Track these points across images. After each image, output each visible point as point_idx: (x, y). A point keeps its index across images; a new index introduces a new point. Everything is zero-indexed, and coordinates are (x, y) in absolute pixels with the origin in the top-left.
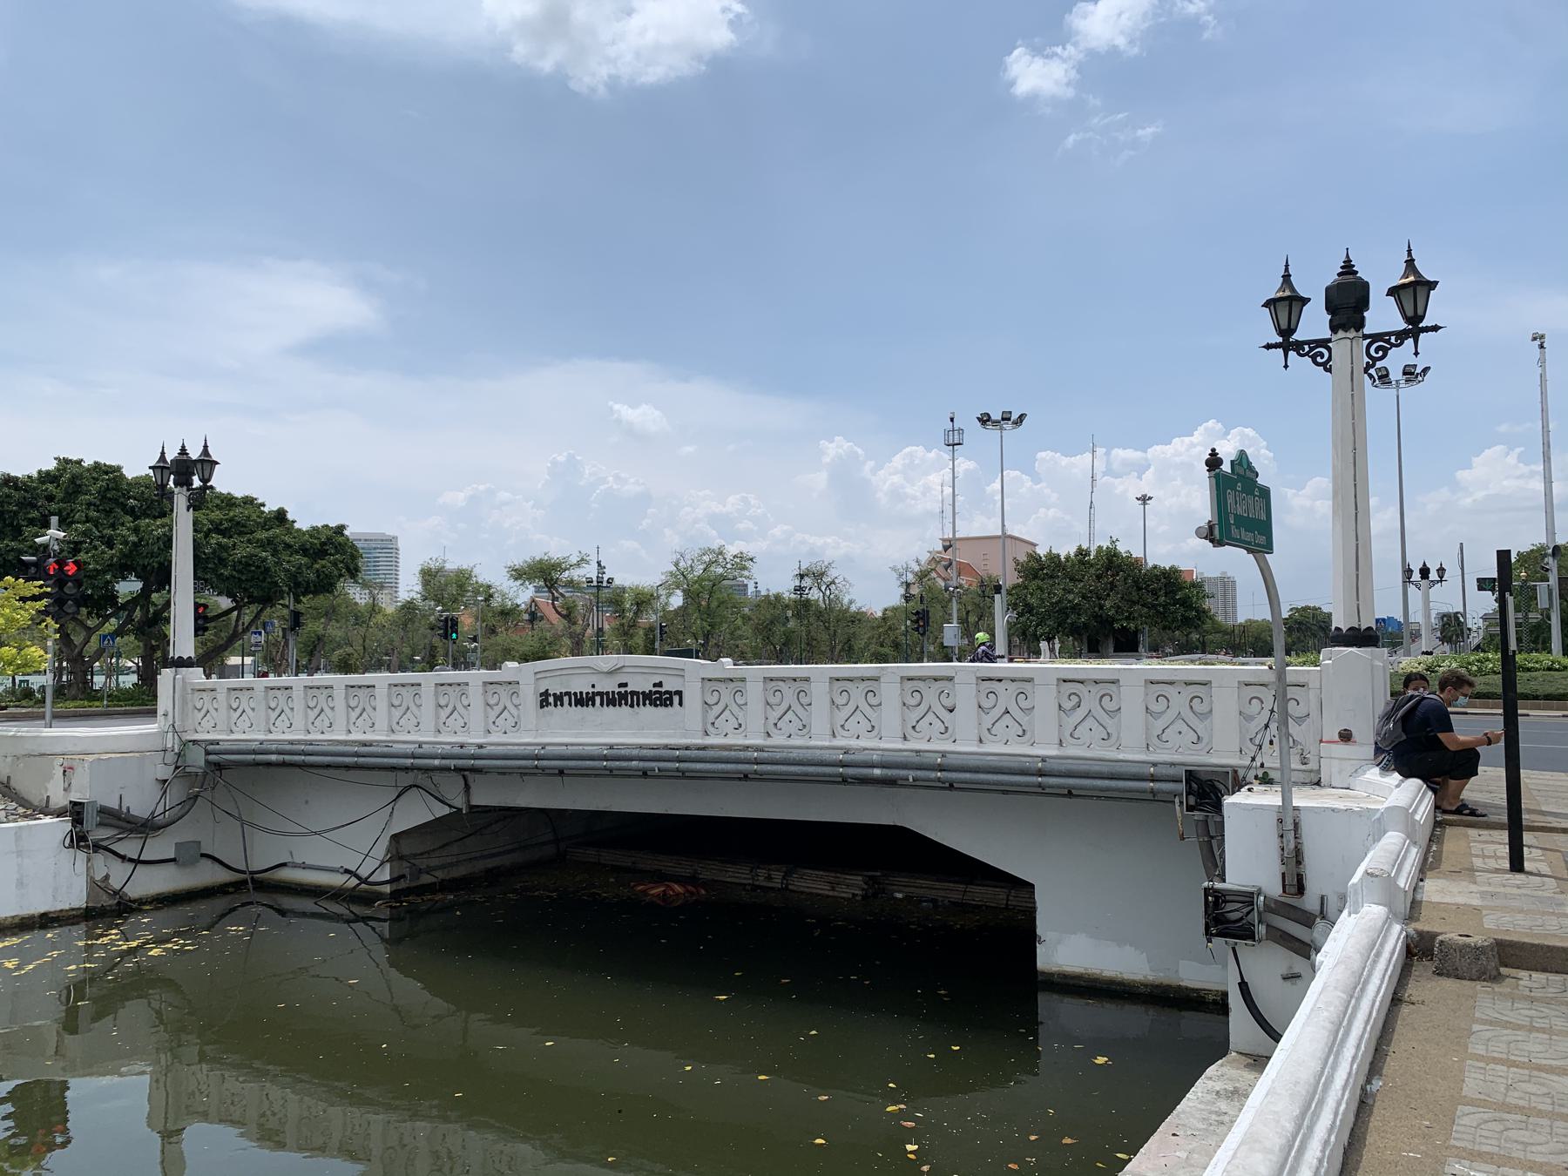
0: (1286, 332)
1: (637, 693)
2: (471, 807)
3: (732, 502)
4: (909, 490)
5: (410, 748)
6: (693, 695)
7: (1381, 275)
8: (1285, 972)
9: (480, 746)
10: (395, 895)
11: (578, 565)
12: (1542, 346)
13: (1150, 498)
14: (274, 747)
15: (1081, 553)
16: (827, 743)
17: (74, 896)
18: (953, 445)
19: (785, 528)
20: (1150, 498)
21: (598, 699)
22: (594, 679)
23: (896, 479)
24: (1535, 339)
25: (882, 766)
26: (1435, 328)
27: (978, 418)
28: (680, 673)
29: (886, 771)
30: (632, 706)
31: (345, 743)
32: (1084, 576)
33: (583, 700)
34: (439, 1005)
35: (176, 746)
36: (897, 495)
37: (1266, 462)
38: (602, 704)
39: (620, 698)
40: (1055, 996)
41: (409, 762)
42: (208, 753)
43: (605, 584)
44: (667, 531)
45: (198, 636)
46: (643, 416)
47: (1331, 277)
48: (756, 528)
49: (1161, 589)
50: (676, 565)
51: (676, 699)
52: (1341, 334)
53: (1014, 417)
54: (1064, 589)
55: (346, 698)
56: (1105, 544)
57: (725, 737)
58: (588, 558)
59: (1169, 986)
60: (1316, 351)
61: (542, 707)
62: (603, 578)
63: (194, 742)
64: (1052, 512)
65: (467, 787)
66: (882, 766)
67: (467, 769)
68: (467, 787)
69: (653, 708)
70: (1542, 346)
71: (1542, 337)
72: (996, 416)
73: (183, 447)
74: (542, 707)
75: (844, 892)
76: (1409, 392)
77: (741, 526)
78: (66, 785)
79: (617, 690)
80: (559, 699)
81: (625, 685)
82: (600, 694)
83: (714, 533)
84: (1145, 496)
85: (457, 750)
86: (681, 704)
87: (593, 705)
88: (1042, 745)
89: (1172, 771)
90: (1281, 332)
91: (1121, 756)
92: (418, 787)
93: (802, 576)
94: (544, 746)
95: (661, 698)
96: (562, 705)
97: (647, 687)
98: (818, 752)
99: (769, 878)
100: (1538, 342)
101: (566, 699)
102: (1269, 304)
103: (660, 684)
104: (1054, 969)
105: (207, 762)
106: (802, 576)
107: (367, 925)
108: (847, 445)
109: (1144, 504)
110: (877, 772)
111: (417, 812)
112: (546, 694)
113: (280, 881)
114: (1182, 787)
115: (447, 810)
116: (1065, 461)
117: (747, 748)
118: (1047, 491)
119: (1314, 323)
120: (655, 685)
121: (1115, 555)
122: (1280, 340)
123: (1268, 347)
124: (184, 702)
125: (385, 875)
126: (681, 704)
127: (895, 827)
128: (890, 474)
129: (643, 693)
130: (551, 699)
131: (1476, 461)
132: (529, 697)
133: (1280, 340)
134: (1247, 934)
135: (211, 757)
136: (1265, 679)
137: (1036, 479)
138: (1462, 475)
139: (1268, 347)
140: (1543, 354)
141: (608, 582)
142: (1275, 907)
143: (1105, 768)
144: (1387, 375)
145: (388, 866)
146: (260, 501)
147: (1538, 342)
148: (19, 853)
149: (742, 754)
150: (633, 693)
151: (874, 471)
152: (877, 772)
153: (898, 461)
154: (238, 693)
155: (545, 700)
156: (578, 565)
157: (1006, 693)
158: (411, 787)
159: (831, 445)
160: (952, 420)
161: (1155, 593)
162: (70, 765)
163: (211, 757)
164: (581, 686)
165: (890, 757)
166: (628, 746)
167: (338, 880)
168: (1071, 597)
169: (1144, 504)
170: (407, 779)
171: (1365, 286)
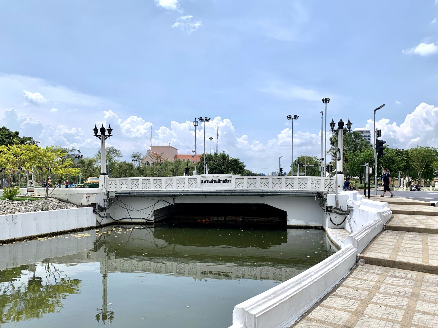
0: (332, 128)
1: (222, 181)
2: (175, 204)
3: (73, 130)
4: (132, 129)
5: (172, 191)
6: (233, 181)
7: (106, 127)
8: (335, 216)
9: (188, 191)
10: (155, 222)
11: (72, 151)
12: (322, 114)
13: (213, 139)
14: (135, 192)
15: (215, 154)
16: (259, 189)
17: (94, 224)
18: (195, 125)
19: (91, 140)
20: (213, 139)
21: (214, 182)
22: (213, 178)
23: (129, 126)
24: (321, 112)
25: (270, 192)
26: (112, 135)
27: (199, 118)
28: (231, 177)
29: (270, 193)
30: (221, 183)
31: (154, 191)
32: (217, 160)
33: (210, 182)
34: (167, 243)
35: (106, 192)
36: (128, 131)
37: (232, 129)
38: (214, 183)
39: (219, 182)
40: (290, 229)
41: (172, 194)
42: (115, 193)
43: (80, 157)
44: (50, 138)
45: (301, 167)
46: (36, 96)
47: (339, 121)
48: (81, 139)
49: (234, 164)
50: (99, 152)
51: (230, 182)
52: (340, 130)
53: (208, 119)
54: (213, 163)
55: (154, 182)
56: (222, 152)
57: (239, 188)
58: (75, 149)
59: (308, 226)
60: (99, 137)
61: (201, 183)
62: (80, 155)
63: (112, 191)
64: (175, 140)
65: (174, 200)
66: (270, 192)
67: (174, 196)
68: (174, 200)
69: (225, 183)
70: (322, 114)
71: (323, 112)
72: (204, 118)
73: (103, 125)
74: (201, 183)
75: (238, 220)
76: (295, 121)
77: (76, 138)
78: (87, 200)
79: (218, 180)
80: (205, 182)
81: (219, 179)
82: (214, 181)
83: (66, 140)
84: (211, 138)
85: (182, 191)
86: (231, 183)
87: (213, 183)
88: (296, 188)
89: (315, 192)
90: (332, 128)
91: (307, 190)
92: (162, 200)
93: (134, 157)
94: (202, 190)
95: (226, 182)
96: (206, 183)
97: (224, 180)
98: (258, 190)
99: (221, 218)
100: (322, 113)
101: (207, 182)
102: (330, 124)
103: (227, 179)
104: (290, 225)
105: (115, 195)
106: (134, 157)
107: (150, 229)
108: (112, 113)
109: (211, 140)
110: (269, 193)
111: (161, 205)
112: (202, 181)
113: (122, 222)
114: (317, 194)
115: (169, 205)
116: (179, 125)
117: (244, 190)
118: (174, 133)
119: (99, 133)
120: (226, 179)
121: (224, 155)
122: (95, 135)
123: (330, 130)
124: (107, 183)
125: (153, 218)
126: (231, 183)
127: (264, 204)
128: (127, 124)
129: (223, 181)
130: (203, 182)
131: (282, 132)
132: (199, 181)
133: (95, 135)
134: (331, 212)
135: (116, 194)
136: (328, 179)
137: (171, 130)
138: (279, 136)
139: (330, 130)
140: (322, 116)
141: (81, 156)
142: (335, 208)
143: (306, 192)
144: (291, 117)
145: (153, 217)
146: (8, 129)
147: (322, 113)
148: (87, 214)
149: (244, 191)
150: (221, 181)
151: (121, 122)
152: (269, 193)
153: (129, 120)
154: (111, 181)
155: (202, 182)
156: (72, 151)
157: (290, 181)
158: (160, 200)
159: (108, 112)
160: (195, 119)
161: (233, 165)
162: (88, 196)
163: (116, 194)
164: (210, 179)
165: (271, 191)
166: (220, 190)
167: (143, 221)
168: (215, 165)
169: (211, 140)
170: (160, 198)
171: (343, 123)
